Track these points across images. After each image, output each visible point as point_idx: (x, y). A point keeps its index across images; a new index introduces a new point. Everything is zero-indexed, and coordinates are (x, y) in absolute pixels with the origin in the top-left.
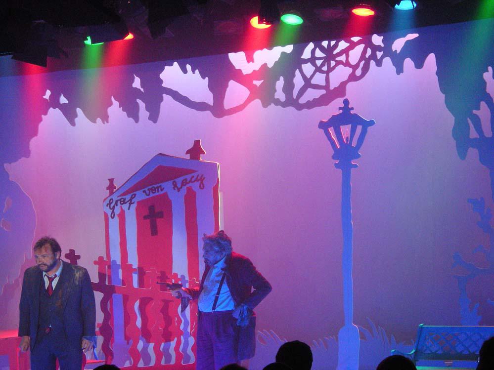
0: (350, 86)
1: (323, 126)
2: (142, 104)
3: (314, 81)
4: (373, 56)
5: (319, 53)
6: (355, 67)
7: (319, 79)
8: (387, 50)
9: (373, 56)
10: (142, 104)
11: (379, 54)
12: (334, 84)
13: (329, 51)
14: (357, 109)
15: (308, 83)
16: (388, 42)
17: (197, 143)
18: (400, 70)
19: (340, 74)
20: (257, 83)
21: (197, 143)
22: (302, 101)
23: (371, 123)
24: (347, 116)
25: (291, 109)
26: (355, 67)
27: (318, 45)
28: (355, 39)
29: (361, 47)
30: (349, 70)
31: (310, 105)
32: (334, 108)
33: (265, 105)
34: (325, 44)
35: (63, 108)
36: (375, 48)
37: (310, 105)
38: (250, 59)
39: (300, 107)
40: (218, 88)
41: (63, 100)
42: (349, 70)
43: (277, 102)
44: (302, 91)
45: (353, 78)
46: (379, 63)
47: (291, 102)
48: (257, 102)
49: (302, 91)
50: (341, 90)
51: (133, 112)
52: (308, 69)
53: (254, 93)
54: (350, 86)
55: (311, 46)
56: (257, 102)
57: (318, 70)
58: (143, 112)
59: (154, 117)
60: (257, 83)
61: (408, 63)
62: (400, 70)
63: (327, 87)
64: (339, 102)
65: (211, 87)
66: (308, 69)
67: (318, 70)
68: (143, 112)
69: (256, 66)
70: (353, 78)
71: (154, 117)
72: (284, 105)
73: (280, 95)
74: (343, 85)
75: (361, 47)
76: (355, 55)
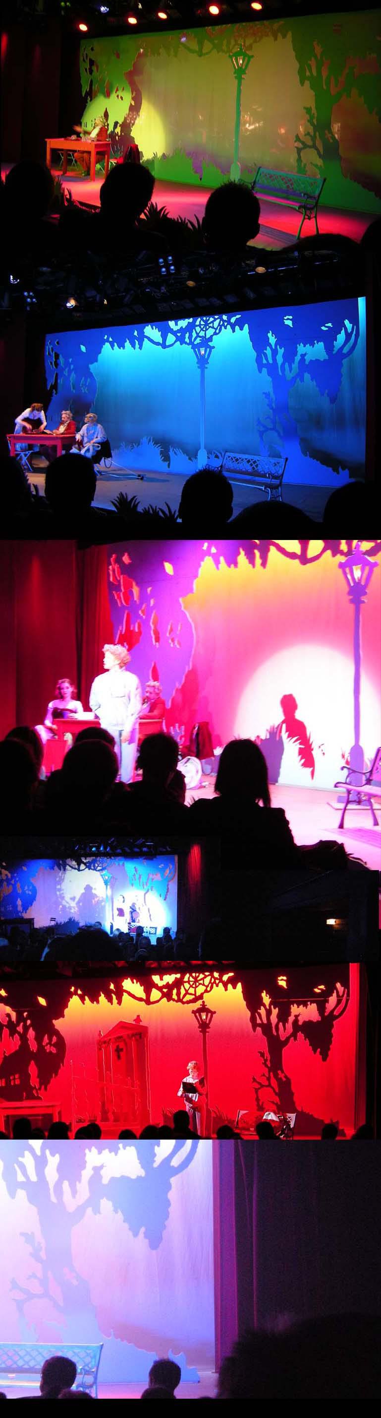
0: (205, 995)
1: (194, 1012)
2: (114, 997)
3: (190, 991)
4: (215, 982)
5: (191, 979)
6: (207, 987)
7: (192, 991)
8: (221, 980)
9: (215, 982)
10: (114, 997)
11: (217, 981)
12: (208, 336)
13: (196, 978)
14: (209, 1005)
15: (187, 993)
16: (229, 319)
17: (138, 1016)
18: (234, 331)
19: (200, 990)
20: (165, 990)
21: (138, 1016)
22: (185, 1000)
23: (215, 1012)
24: (204, 1009)
25: (180, 1003)
26: (207, 987)
27: (202, 319)
28: (207, 974)
29: (209, 978)
30: (204, 988)
31: (188, 1002)
32: (198, 1004)
33: (169, 1001)
34: (194, 975)
35: (80, 996)
36: (216, 979)
37: (188, 1002)
38: (161, 979)
39: (183, 1003)
40: (148, 992)
41: (79, 992)
42: (204, 988)
43: (174, 1000)
44: (184, 996)
45: (206, 991)
46: (226, 328)
47: (179, 1000)
48: (178, 343)
49: (184, 996)
50: (201, 997)
51: (110, 1000)
52: (198, 329)
53: (164, 995)
54: (205, 995)
55: (188, 975)
56: (178, 343)
57: (202, 330)
58: (137, 346)
59: (120, 1003)
60: (165, 990)
61: (237, 328)
62: (234, 331)
63: (195, 994)
64: (200, 1002)
65: (145, 991)
66: (187, 986)
67: (202, 330)
68: (137, 346)
69: (178, 328)
70: (206, 991)
71: (120, 1003)
72: (177, 1001)
73: (175, 997)
74: (202, 994)
75: (209, 978)
76: (216, 324)
